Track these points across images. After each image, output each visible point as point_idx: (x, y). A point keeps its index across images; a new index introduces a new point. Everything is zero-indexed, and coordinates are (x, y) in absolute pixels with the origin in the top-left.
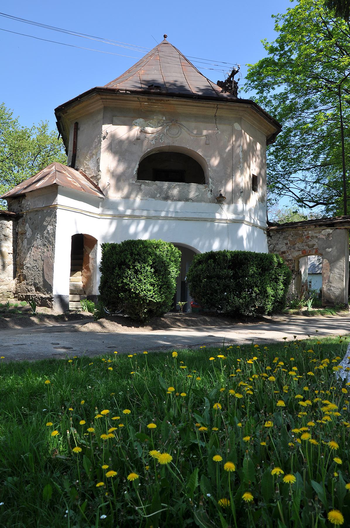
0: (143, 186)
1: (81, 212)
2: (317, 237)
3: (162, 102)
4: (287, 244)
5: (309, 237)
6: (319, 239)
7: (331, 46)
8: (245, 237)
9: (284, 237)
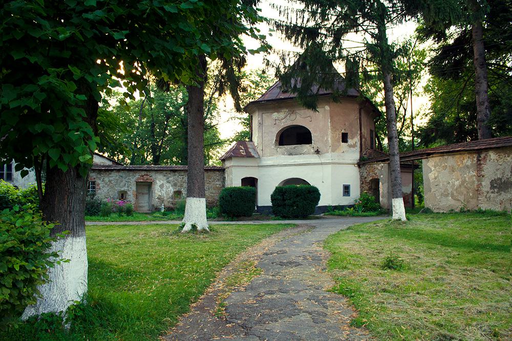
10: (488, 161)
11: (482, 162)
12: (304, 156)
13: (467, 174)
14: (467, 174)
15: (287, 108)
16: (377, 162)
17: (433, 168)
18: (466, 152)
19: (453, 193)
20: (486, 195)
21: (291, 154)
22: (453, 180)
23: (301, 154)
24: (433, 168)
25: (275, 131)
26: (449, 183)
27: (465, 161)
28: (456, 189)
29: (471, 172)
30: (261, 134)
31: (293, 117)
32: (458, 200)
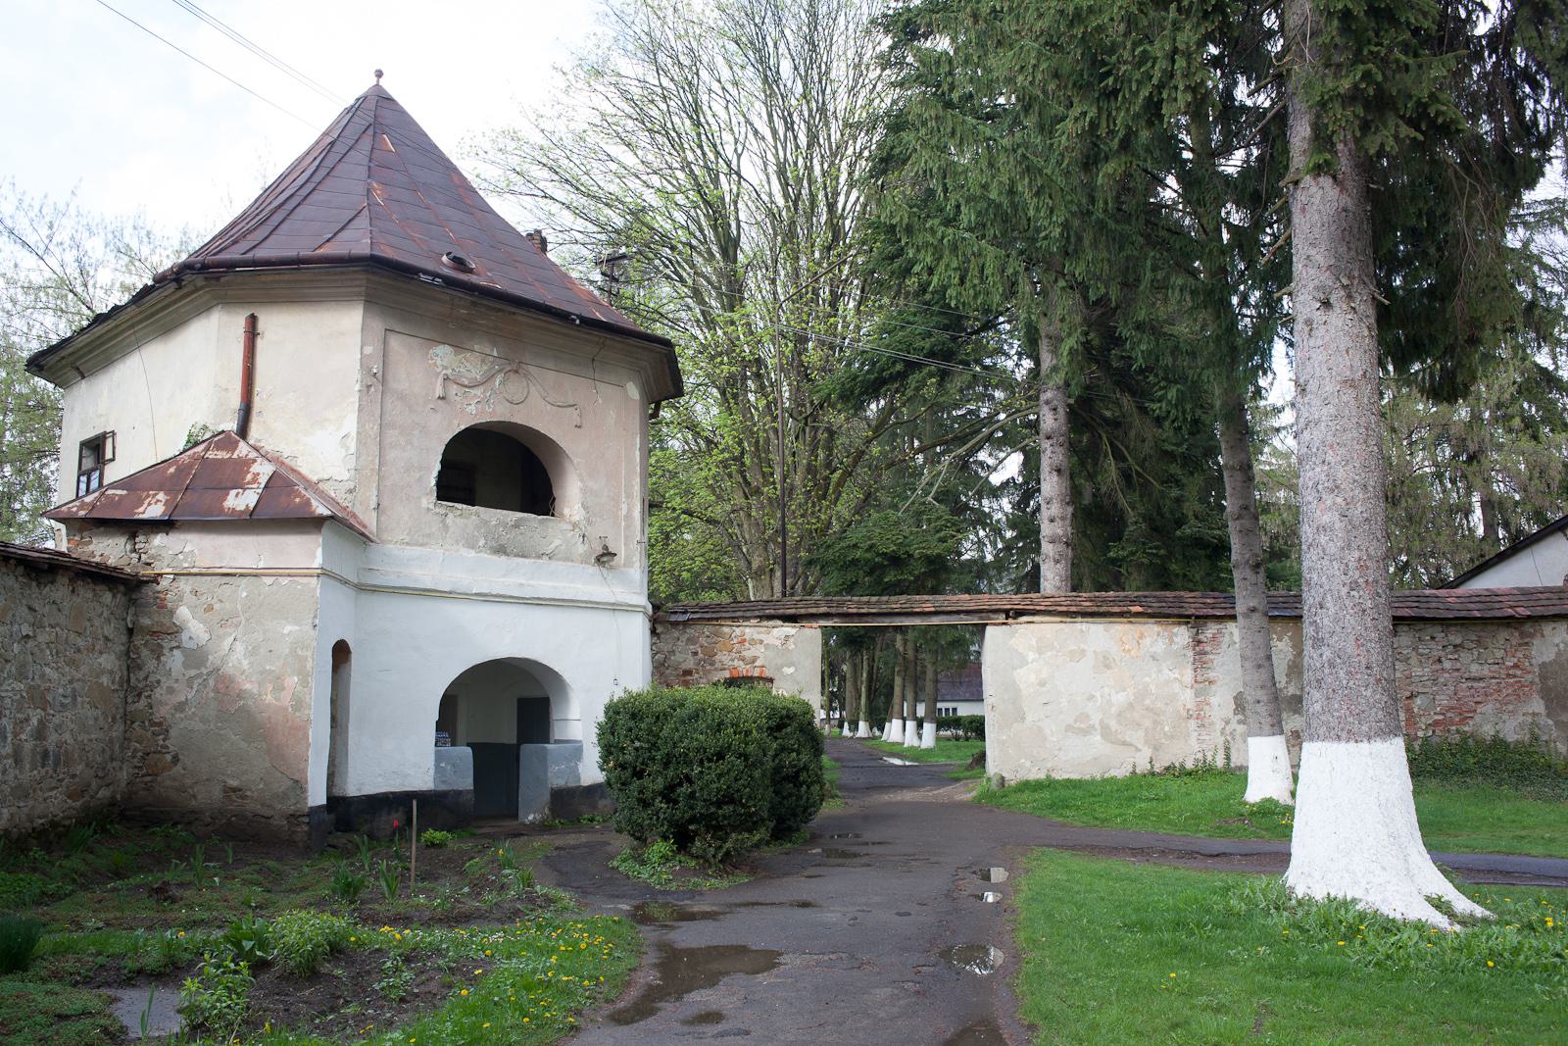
0: (450, 520)
1: (114, 448)
2: (761, 642)
3: (500, 314)
4: (695, 654)
5: (745, 640)
6: (767, 646)
7: (14, 615)
8: (815, 699)
9: (688, 639)
10: (1224, 646)
11: (1208, 649)
12: (555, 565)
13: (1154, 676)
14: (1154, 676)
15: (494, 344)
16: (761, 618)
17: (1031, 656)
18: (1153, 620)
19: (1108, 727)
20: (1224, 729)
21: (501, 550)
22: (1106, 689)
23: (540, 556)
24: (1031, 656)
25: (445, 428)
26: (1091, 697)
27: (1147, 641)
28: (1119, 715)
29: (1166, 671)
30: (373, 429)
31: (516, 387)
32: (1124, 743)
